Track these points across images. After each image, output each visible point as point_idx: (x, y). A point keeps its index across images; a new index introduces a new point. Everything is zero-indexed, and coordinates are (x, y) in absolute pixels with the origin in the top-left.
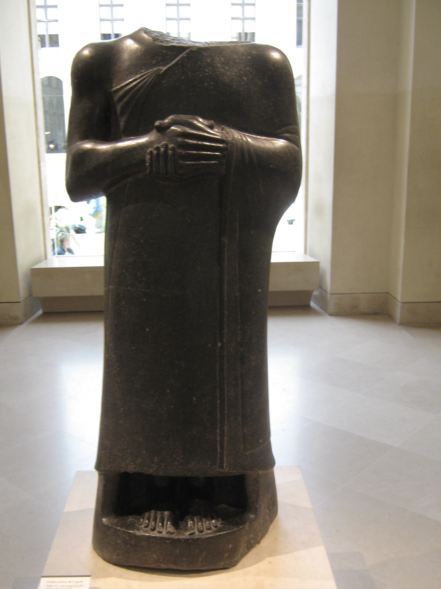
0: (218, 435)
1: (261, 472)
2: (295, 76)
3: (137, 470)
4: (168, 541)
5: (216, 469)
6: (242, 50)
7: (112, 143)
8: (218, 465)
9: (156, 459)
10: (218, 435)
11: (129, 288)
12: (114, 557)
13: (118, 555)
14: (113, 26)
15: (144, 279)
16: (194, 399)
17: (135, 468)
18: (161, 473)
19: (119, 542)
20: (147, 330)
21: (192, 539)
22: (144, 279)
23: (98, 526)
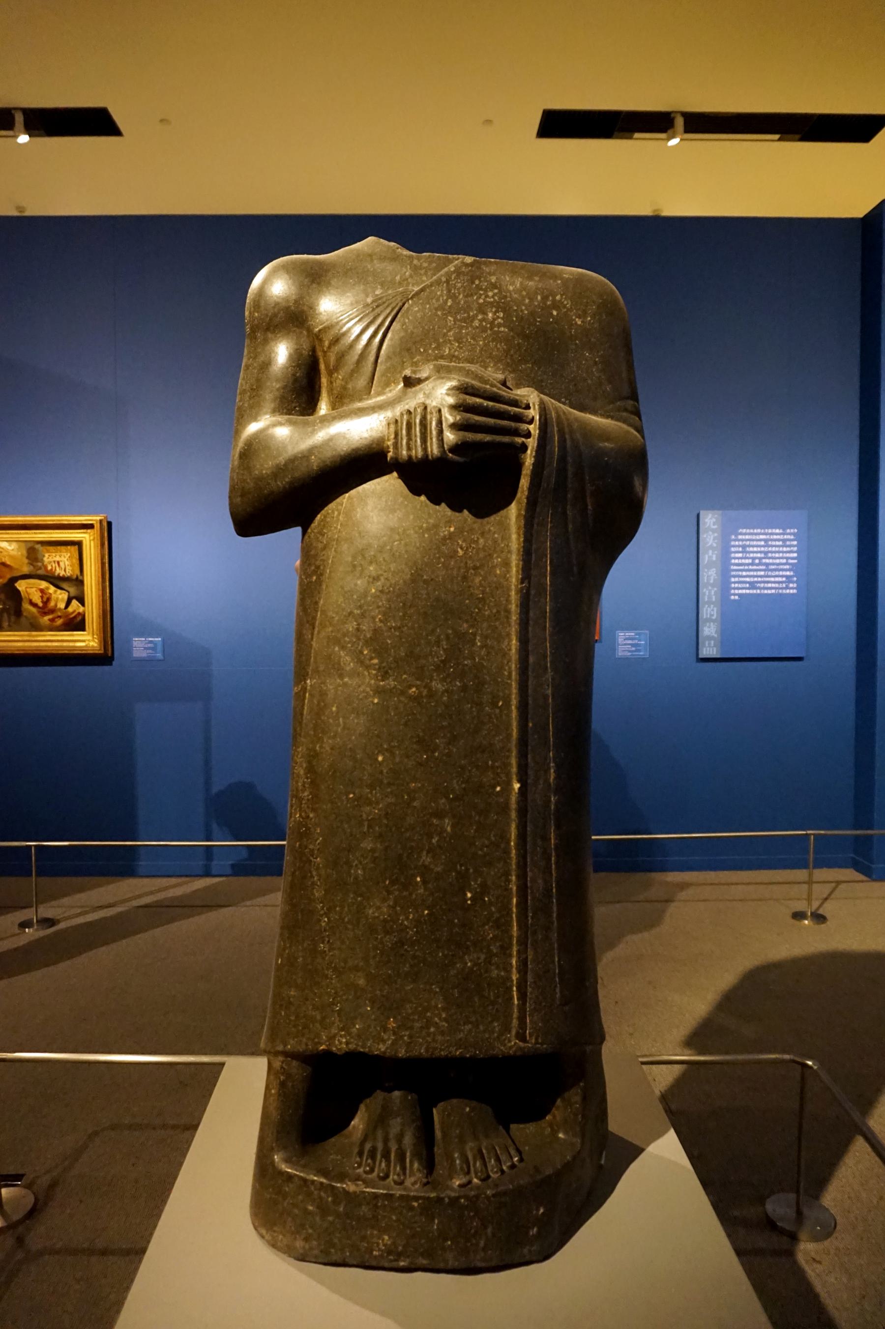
0: (514, 970)
1: (589, 1048)
2: (15, 213)
3: (352, 1047)
4: (415, 1204)
5: (510, 1041)
6: (273, 355)
7: (320, 387)
8: (514, 1032)
9: (392, 1023)
10: (514, 970)
11: (346, 680)
12: (299, 1244)
13: (306, 1239)
14: (804, 883)
15: (376, 661)
16: (469, 895)
17: (347, 1043)
18: (402, 1053)
19: (311, 1208)
20: (380, 758)
21: (466, 1197)
22: (376, 661)
23: (264, 1170)
